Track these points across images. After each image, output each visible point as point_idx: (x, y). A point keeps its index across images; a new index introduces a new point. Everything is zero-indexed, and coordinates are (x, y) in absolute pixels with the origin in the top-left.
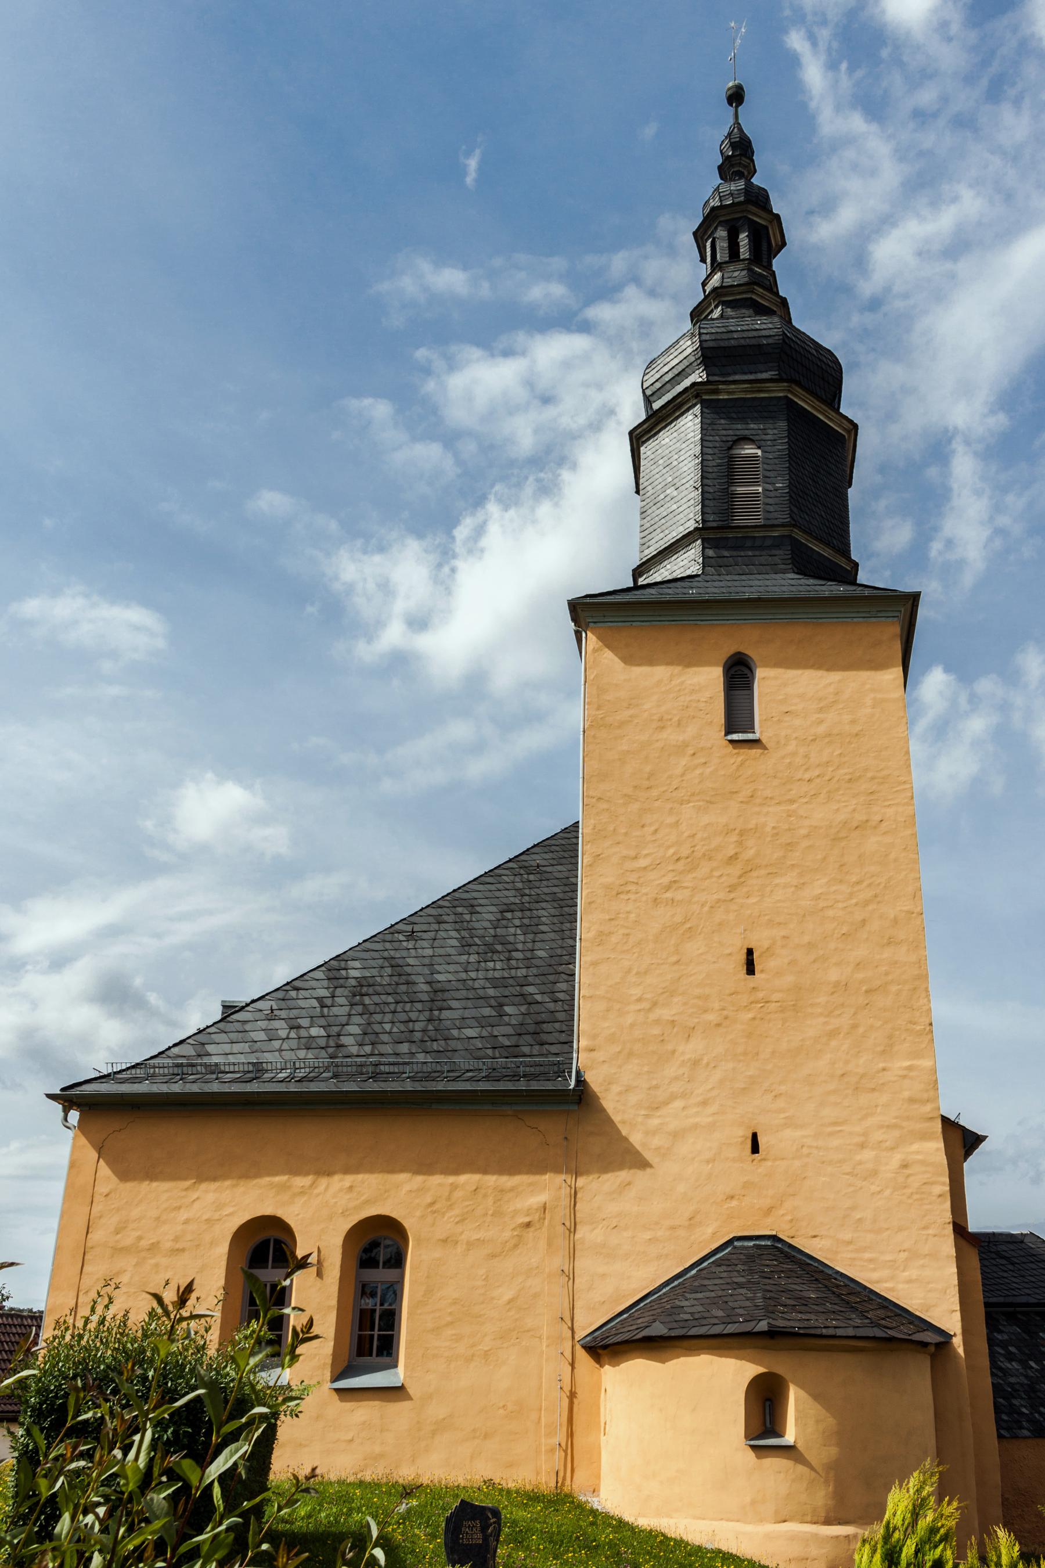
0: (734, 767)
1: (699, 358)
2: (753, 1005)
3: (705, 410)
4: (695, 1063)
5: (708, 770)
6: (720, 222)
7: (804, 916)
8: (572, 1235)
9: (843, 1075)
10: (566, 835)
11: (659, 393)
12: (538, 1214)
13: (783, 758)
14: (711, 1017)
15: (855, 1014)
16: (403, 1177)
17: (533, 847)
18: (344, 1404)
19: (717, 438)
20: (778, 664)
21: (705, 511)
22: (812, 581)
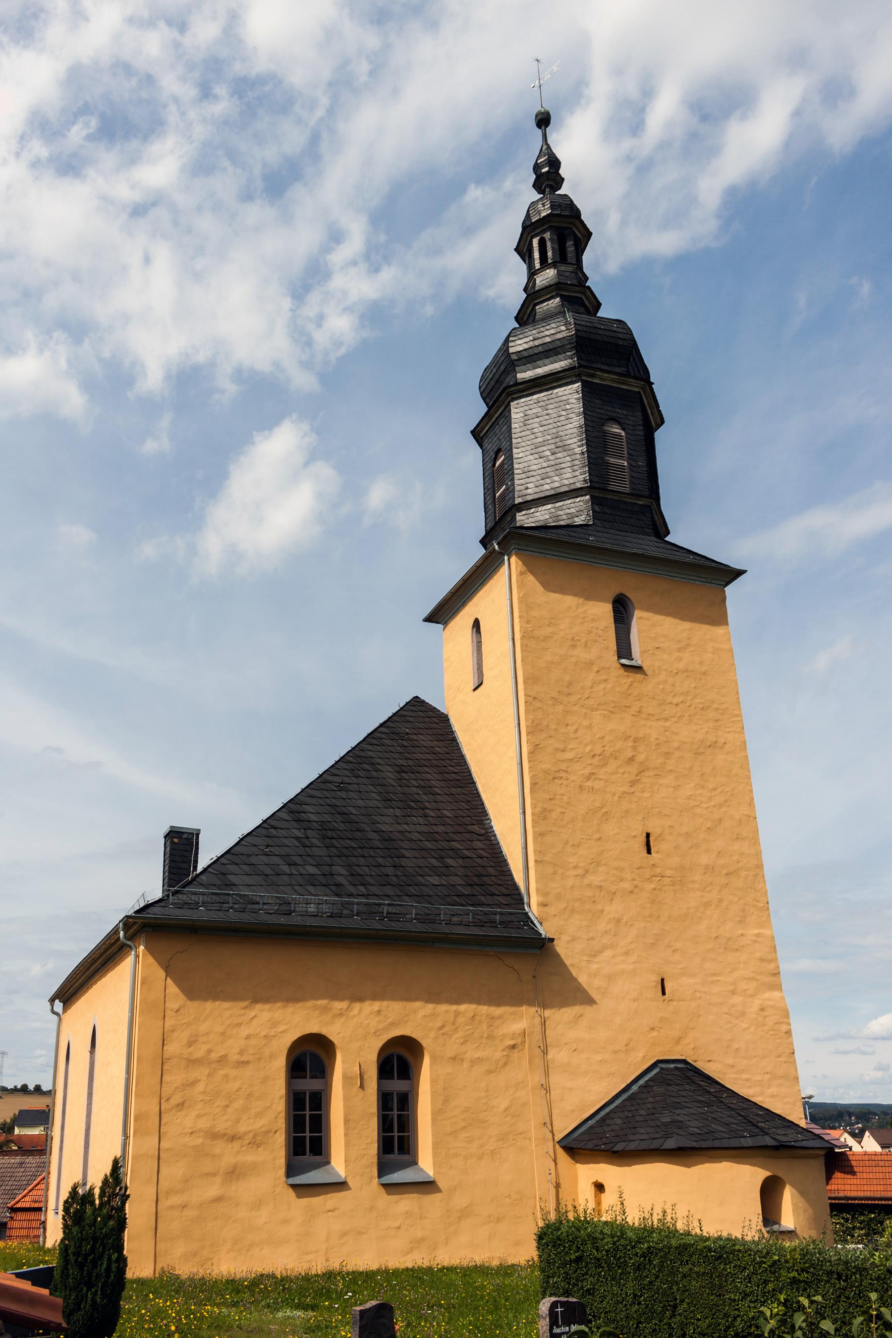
0: (626, 686)
1: (573, 343)
2: (653, 878)
4: (618, 921)
5: (609, 686)
6: (551, 226)
9: (716, 937)
10: (413, 708)
13: (658, 684)
14: (626, 885)
15: (720, 891)
16: (418, 1004)
19: (594, 414)
20: (648, 609)
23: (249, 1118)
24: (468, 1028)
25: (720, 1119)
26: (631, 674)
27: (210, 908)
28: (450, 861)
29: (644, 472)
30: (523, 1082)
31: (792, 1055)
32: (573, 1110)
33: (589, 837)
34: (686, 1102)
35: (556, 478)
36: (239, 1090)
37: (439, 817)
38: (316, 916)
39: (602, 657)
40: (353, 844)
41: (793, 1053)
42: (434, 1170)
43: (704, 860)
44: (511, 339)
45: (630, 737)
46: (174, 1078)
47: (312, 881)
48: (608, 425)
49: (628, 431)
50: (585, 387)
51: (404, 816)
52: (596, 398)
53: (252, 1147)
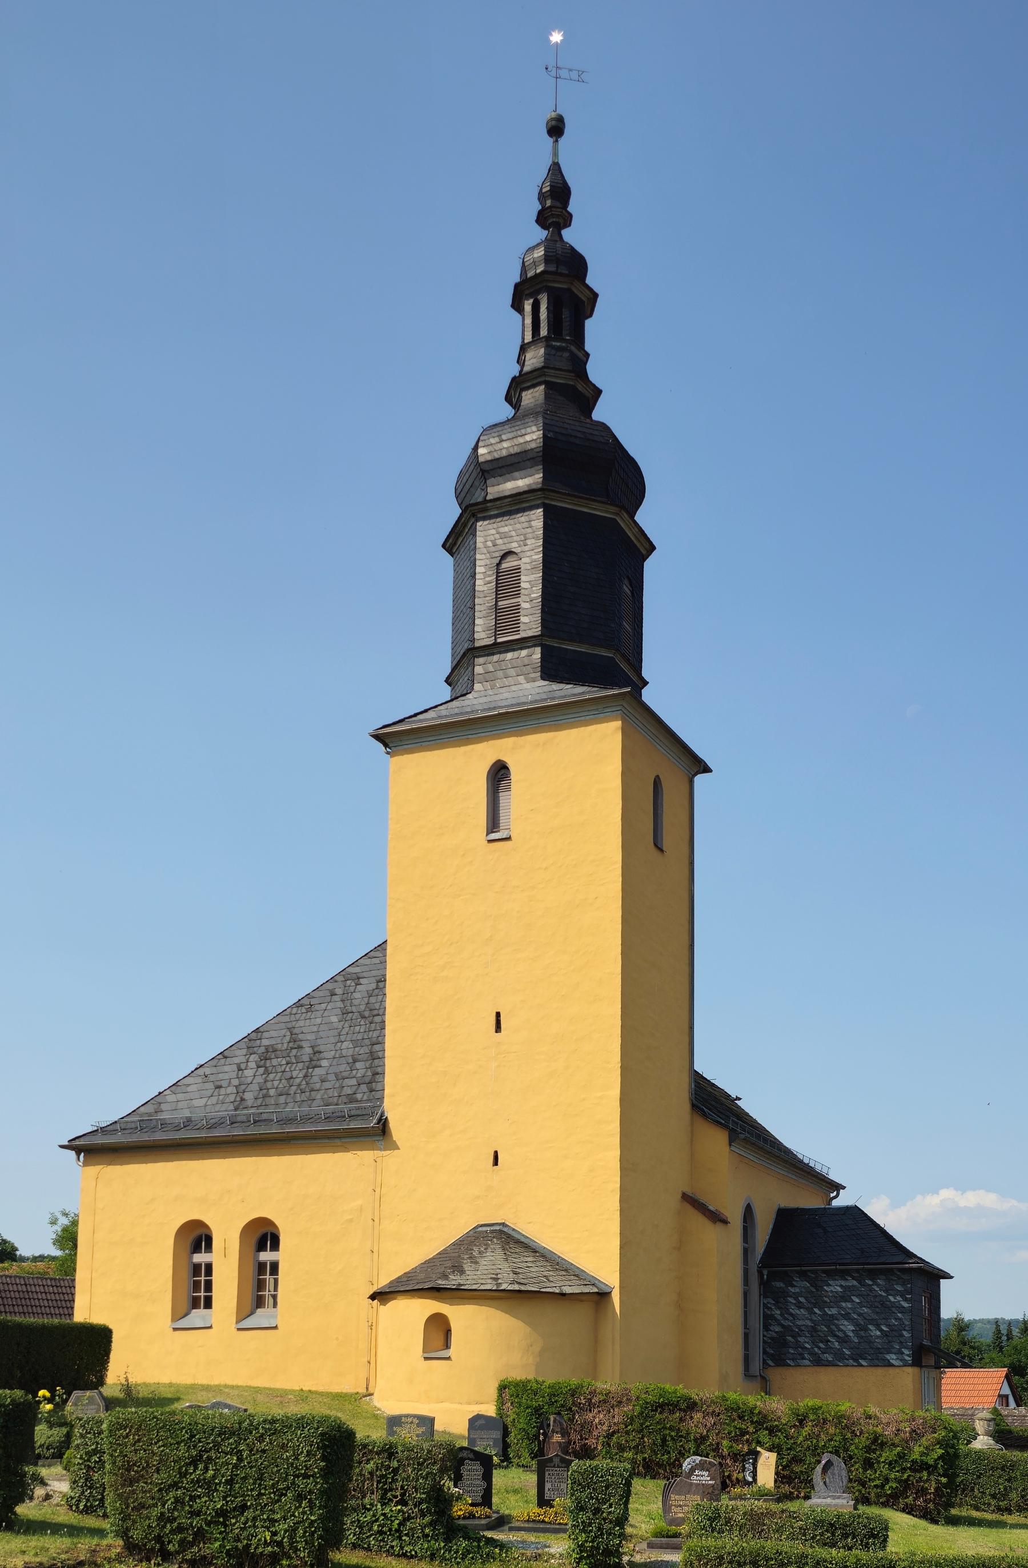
22: (562, 686)
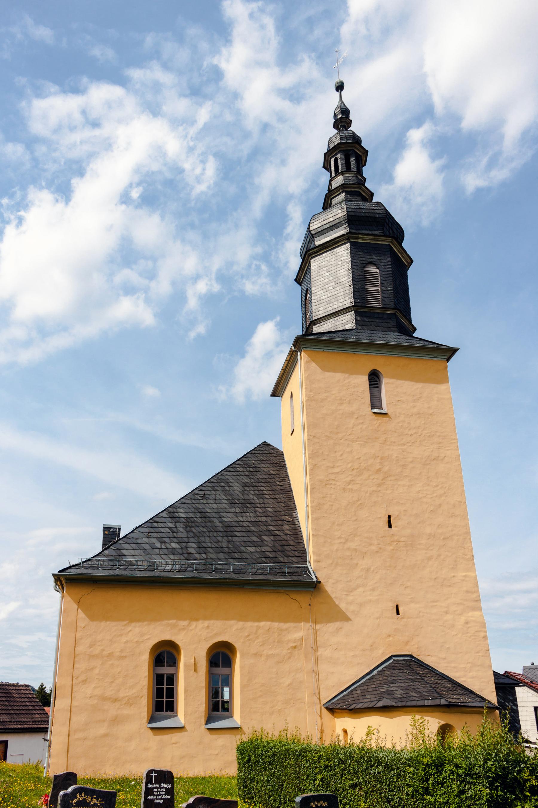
0: (376, 426)
1: (346, 220)
2: (393, 543)
3: (352, 247)
4: (368, 570)
5: (364, 426)
6: (341, 150)
7: (413, 501)
8: (316, 653)
9: (436, 578)
10: (261, 449)
11: (322, 232)
12: (299, 642)
13: (399, 423)
14: (374, 548)
15: (439, 549)
16: (233, 622)
17: (247, 454)
18: (212, 736)
19: (358, 261)
20: (392, 377)
21: (355, 297)
23: (126, 689)
24: (265, 636)
25: (417, 690)
26: (380, 418)
27: (105, 569)
28: (265, 538)
29: (391, 293)
30: (301, 668)
31: (487, 652)
32: (334, 686)
33: (349, 519)
34: (400, 680)
35: (336, 303)
36: (119, 673)
37: (265, 512)
38: (170, 571)
39: (360, 409)
40: (205, 530)
41: (488, 650)
42: (241, 721)
43: (428, 530)
44: (312, 222)
45: (379, 456)
46: (81, 666)
47: (173, 551)
48: (370, 267)
49: (381, 269)
50: (352, 245)
51: (241, 512)
52: (360, 252)
53: (127, 706)
